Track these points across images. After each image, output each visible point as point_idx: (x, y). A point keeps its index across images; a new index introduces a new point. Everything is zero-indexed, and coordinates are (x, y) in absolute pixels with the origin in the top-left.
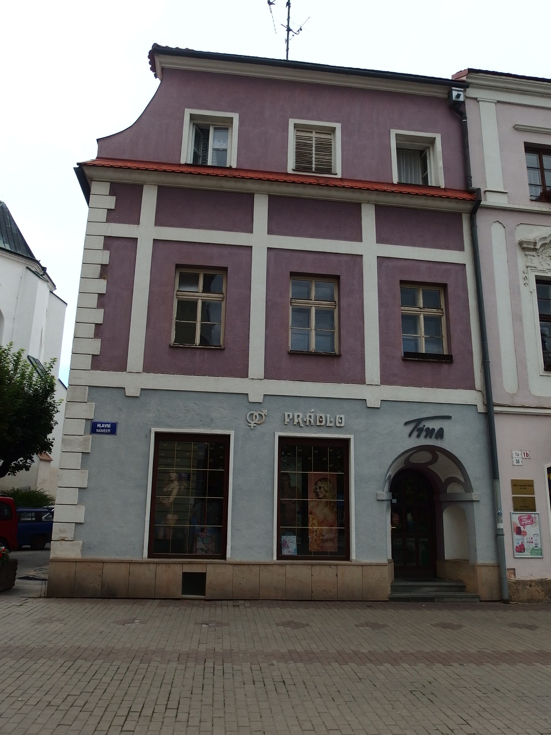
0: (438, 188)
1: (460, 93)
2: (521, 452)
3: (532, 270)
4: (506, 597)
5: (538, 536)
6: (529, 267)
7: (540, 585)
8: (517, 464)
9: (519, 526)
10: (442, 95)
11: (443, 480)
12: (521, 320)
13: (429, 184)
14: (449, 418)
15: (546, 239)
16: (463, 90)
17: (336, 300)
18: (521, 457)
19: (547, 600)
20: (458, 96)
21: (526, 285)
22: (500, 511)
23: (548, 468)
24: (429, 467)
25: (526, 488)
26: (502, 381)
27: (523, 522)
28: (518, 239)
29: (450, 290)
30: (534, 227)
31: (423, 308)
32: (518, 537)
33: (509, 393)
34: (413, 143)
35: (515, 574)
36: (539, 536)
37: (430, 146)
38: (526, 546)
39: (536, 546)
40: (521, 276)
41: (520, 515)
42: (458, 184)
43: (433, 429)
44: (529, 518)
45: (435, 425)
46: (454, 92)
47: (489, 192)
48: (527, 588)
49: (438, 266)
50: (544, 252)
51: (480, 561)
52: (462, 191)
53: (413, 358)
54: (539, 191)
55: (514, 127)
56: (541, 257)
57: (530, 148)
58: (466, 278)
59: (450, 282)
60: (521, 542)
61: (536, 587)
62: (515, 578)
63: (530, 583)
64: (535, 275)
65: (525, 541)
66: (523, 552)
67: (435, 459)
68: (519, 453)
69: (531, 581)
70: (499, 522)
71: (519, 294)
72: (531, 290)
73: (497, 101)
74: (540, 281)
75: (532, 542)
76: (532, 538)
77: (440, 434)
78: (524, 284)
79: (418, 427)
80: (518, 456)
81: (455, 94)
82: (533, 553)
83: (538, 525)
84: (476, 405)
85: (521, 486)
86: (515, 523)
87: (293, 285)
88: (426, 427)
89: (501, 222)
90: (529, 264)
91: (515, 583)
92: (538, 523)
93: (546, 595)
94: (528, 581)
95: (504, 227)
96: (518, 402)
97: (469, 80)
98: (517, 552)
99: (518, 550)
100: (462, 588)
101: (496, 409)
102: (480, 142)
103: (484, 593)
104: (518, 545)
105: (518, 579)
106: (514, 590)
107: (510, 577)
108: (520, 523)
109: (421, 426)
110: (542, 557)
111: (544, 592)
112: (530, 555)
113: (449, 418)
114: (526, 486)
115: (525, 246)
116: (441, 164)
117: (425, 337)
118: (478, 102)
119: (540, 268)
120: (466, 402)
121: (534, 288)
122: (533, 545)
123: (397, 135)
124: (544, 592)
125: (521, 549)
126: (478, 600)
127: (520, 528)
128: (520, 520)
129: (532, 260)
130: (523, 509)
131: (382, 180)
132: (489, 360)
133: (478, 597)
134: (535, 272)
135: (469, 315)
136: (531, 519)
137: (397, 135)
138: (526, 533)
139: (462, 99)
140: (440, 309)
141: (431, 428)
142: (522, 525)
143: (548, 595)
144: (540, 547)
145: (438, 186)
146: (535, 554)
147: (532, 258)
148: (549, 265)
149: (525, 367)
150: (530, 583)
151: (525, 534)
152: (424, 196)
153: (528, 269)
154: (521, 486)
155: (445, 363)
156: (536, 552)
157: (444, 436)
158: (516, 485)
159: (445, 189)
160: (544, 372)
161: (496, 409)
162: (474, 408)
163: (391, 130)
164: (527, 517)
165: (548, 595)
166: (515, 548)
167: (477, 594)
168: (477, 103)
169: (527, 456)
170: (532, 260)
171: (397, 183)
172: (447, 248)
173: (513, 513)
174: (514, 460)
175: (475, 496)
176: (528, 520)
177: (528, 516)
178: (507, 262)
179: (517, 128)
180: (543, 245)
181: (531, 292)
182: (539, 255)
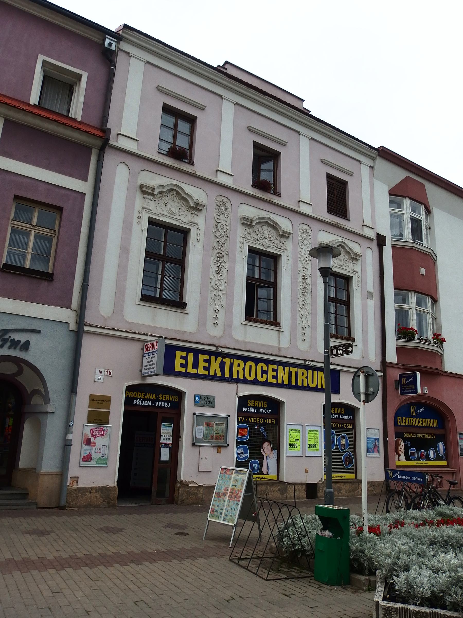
0: (74, 120)
1: (112, 42)
2: (104, 370)
3: (147, 212)
4: (63, 503)
5: (106, 447)
6: (144, 208)
7: (99, 491)
8: (99, 381)
9: (90, 437)
10: (99, 40)
11: (29, 392)
12: (128, 253)
13: (70, 116)
14: (38, 332)
15: (164, 187)
16: (116, 40)
17: (57, 229)
18: (104, 374)
19: (103, 505)
20: (110, 44)
21: (139, 223)
22: (71, 423)
23: (127, 387)
24: (16, 378)
25: (103, 403)
26: (98, 305)
27: (94, 434)
28: (139, 182)
29: (64, 214)
30: (156, 175)
31: (36, 226)
32: (87, 447)
33: (103, 316)
34: (61, 74)
35: (77, 482)
36: (108, 447)
37: (77, 82)
38: (92, 457)
39: (103, 456)
40: (136, 214)
41: (93, 427)
42: (95, 121)
43: (19, 341)
44: (101, 431)
45: (22, 338)
46: (107, 39)
47: (121, 136)
48: (86, 495)
49: (57, 190)
50: (160, 199)
51: (44, 470)
52: (97, 128)
53: (15, 271)
54: (167, 147)
55: (321, 160)
56: (157, 202)
57: (167, 109)
58: (84, 206)
59: (67, 207)
60: (89, 452)
61: (96, 493)
62: (77, 485)
63: (91, 490)
64: (149, 217)
65: (93, 451)
66: (90, 462)
67: (20, 372)
68: (103, 370)
69: (92, 488)
70: (68, 433)
71: (131, 230)
72: (143, 229)
73: (147, 61)
74: (152, 222)
75: (100, 453)
76: (100, 449)
77: (26, 346)
78: (137, 222)
79: (4, 338)
80: (100, 373)
81: (107, 41)
82: (99, 462)
83: (108, 437)
84: (69, 323)
85: (98, 401)
86: (86, 435)
87: (16, 209)
88: (12, 338)
89: (127, 164)
90: (145, 206)
91: (75, 490)
92: (109, 436)
93: (104, 500)
94: (89, 488)
95: (129, 170)
96: (111, 324)
97: (124, 35)
98: (83, 461)
99: (85, 459)
100: (25, 496)
101: (86, 328)
102: (124, 91)
103: (42, 500)
104: (85, 455)
105: (80, 487)
106: (73, 497)
107: (73, 484)
108: (91, 435)
109: (7, 336)
110: (106, 466)
111: (103, 498)
112: (95, 464)
113: (38, 332)
114: (103, 401)
115: (144, 189)
116: (82, 99)
117: (32, 254)
118: (130, 57)
119: (154, 211)
120: (59, 319)
121: (145, 227)
122: (100, 455)
123: (44, 61)
124: (103, 498)
125: (88, 458)
126: (35, 507)
127: (90, 439)
128: (92, 432)
129: (148, 202)
130: (96, 422)
131: (18, 97)
132: (88, 283)
133: (36, 504)
134: (150, 214)
135: (79, 240)
136: (103, 431)
137: (44, 61)
138: (96, 443)
139: (113, 47)
140: (53, 230)
141: (16, 340)
142: (93, 437)
143: (106, 500)
144: (107, 457)
145: (75, 118)
146: (101, 463)
147: (149, 201)
148: (163, 211)
149: (123, 295)
150: (91, 490)
151: (94, 444)
152: (5, 105)
153: (143, 210)
154: (98, 401)
155: (46, 280)
156: (102, 461)
157: (30, 349)
158: (94, 400)
159: (80, 123)
160: (140, 301)
161: (86, 328)
162: (66, 325)
163: (39, 55)
164: (99, 429)
165: (106, 500)
166: (82, 457)
167: (35, 501)
168: (129, 58)
169: (109, 374)
170: (148, 202)
171: (33, 104)
172: (71, 175)
173: (86, 425)
174: (97, 377)
175: (50, 408)
176: (100, 432)
177: (100, 429)
178: (125, 200)
179: (160, 89)
180: (258, 223)
181: (142, 230)
182: (156, 200)
